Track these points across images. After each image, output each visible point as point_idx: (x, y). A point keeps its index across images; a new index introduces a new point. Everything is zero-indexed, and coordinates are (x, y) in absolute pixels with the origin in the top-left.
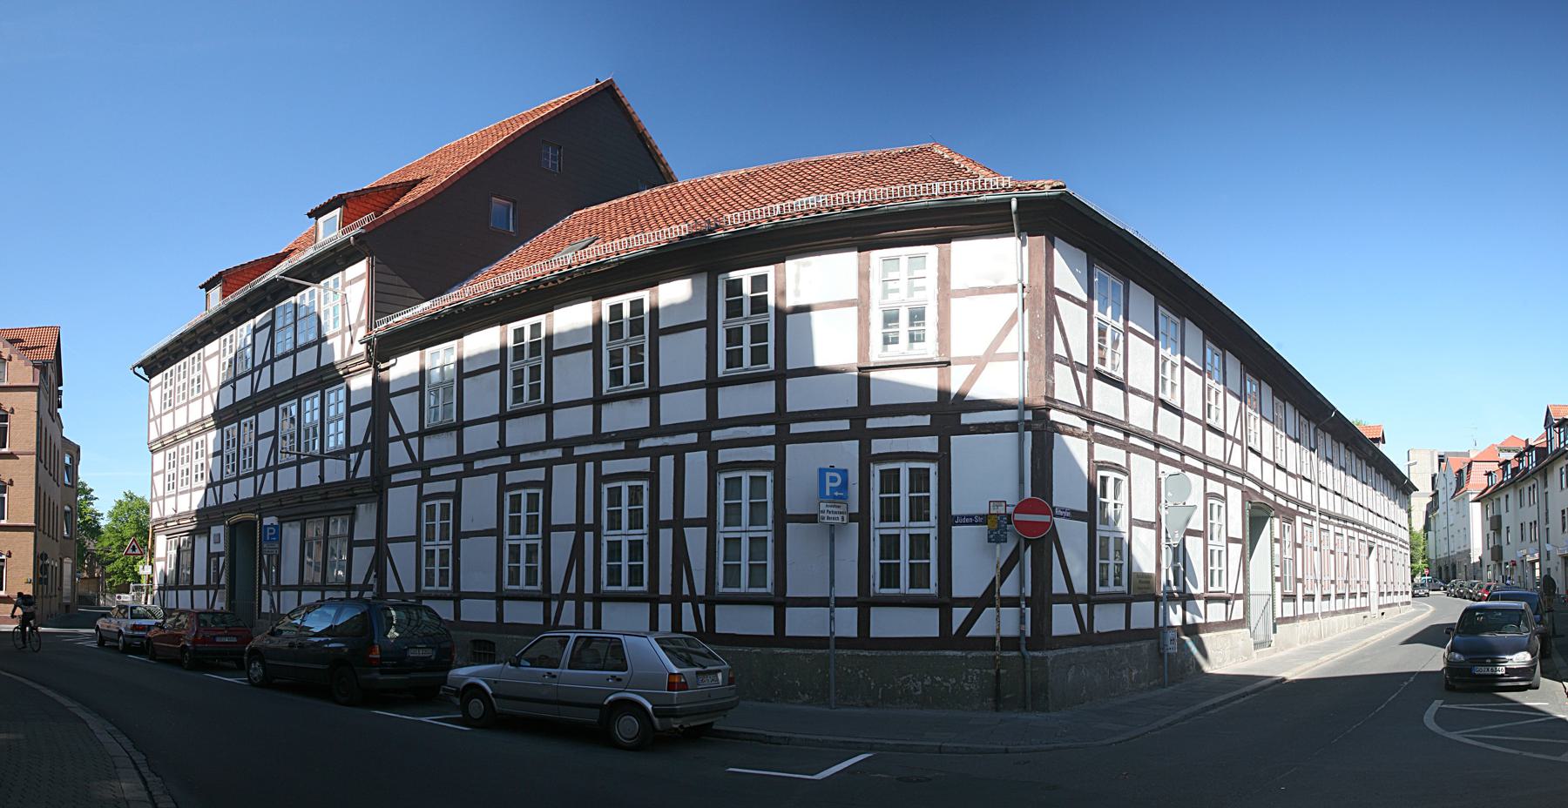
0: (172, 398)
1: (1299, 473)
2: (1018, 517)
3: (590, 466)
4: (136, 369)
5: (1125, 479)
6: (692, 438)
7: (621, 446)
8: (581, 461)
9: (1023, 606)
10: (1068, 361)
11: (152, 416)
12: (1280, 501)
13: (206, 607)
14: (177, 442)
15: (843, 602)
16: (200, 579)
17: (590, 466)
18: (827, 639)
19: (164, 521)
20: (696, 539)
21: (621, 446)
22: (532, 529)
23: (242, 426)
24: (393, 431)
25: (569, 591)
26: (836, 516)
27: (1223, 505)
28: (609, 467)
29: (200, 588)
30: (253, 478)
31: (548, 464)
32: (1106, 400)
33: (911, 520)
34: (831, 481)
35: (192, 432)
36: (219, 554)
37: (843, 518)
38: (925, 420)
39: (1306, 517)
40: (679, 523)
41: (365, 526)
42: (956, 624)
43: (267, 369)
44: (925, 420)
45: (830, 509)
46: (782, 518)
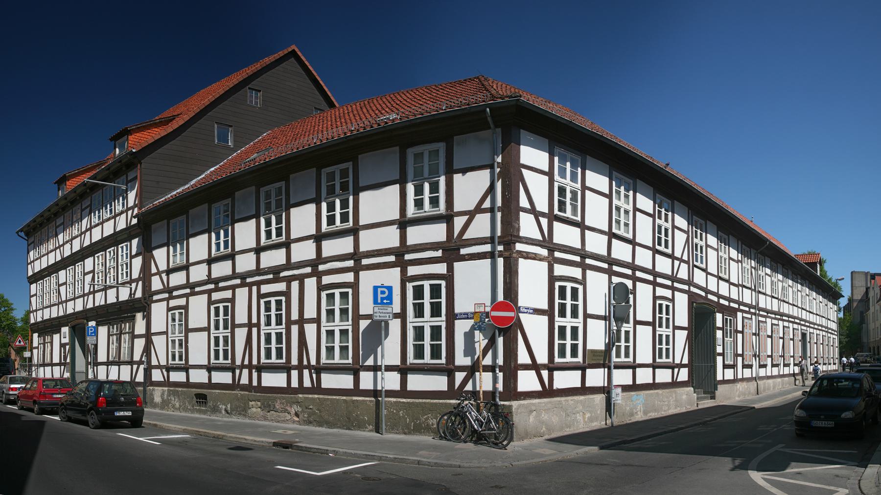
1: (740, 283)
2: (494, 314)
3: (254, 288)
5: (581, 288)
6: (308, 270)
7: (271, 276)
8: (250, 285)
9: (498, 372)
10: (533, 211)
11: (29, 261)
12: (722, 301)
13: (59, 377)
16: (56, 360)
17: (254, 288)
20: (310, 330)
21: (271, 276)
22: (279, 323)
24: (154, 270)
25: (245, 364)
26: (385, 315)
27: (671, 305)
28: (265, 289)
29: (56, 365)
30: (82, 298)
31: (233, 288)
32: (566, 235)
33: (432, 316)
36: (66, 344)
38: (439, 253)
39: (746, 313)
40: (302, 321)
41: (140, 327)
42: (458, 383)
43: (88, 233)
44: (439, 253)
45: (381, 311)
46: (587, 316)
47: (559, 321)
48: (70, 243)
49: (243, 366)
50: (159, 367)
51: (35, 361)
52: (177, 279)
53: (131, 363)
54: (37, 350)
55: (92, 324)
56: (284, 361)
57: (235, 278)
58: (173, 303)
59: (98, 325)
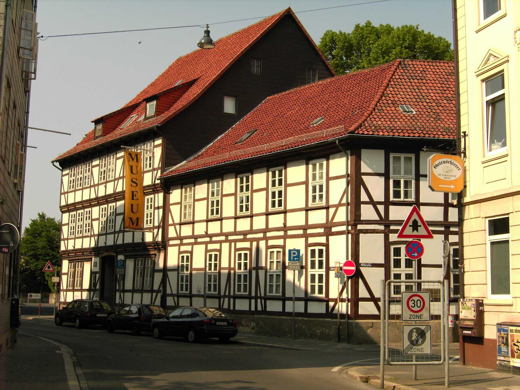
0: (74, 184)
3: (233, 244)
4: (55, 163)
6: (261, 235)
8: (230, 242)
14: (76, 209)
15: (290, 299)
17: (233, 244)
18: (292, 313)
19: (67, 252)
23: (90, 184)
24: (171, 222)
26: (295, 267)
29: (85, 290)
31: (221, 242)
34: (399, 197)
35: (84, 205)
37: (298, 268)
45: (293, 265)
47: (394, 271)
48: (105, 185)
49: (225, 296)
50: (172, 295)
51: (64, 286)
52: (186, 231)
53: (152, 291)
54: (66, 276)
55: (121, 257)
56: (247, 293)
57: (223, 235)
58: (183, 248)
59: (126, 257)
